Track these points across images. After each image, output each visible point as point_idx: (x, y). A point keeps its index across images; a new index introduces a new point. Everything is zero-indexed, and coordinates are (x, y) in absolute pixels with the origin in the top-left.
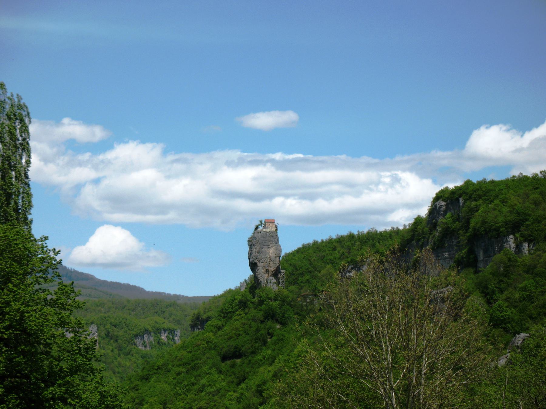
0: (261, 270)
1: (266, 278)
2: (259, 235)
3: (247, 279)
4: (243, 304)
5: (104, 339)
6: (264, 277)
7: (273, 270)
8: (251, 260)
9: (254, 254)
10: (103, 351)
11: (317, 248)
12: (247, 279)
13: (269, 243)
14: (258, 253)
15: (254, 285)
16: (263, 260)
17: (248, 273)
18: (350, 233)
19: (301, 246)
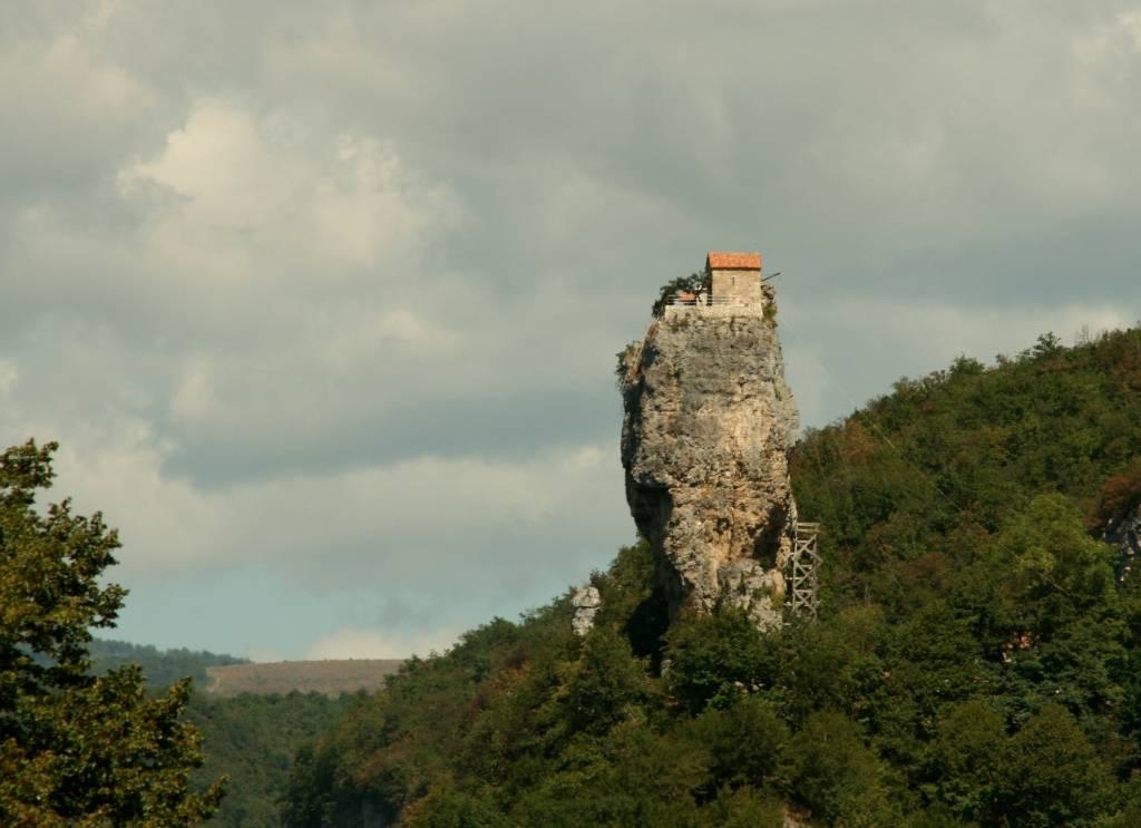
0: (688, 520)
1: (715, 565)
2: (681, 339)
3: (1109, 331)
4: (591, 711)
5: (1007, 748)
6: (708, 559)
7: (754, 520)
8: (637, 470)
9: (652, 439)
10: (179, 713)
11: (977, 401)
12: (1109, 331)
13: (734, 379)
14: (675, 431)
15: (649, 596)
16: (699, 469)
17: (628, 534)
18: (1118, 331)
19: (890, 392)
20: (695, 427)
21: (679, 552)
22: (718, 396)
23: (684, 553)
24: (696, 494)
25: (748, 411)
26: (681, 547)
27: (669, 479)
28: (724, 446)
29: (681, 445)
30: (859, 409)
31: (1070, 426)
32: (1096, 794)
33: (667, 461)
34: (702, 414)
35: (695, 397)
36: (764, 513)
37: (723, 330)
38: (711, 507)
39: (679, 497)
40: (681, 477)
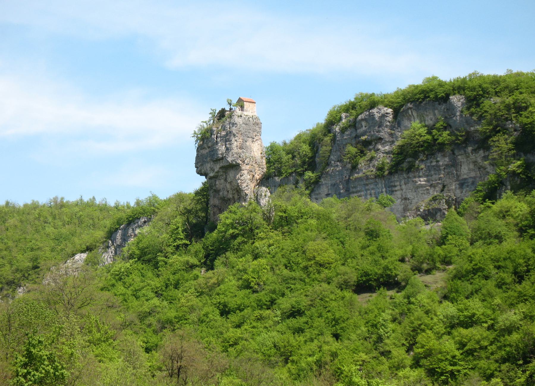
14: (241, 148)
20: (246, 147)
21: (242, 184)
22: (251, 139)
23: (244, 185)
24: (248, 167)
25: (257, 144)
26: (244, 183)
27: (241, 162)
28: (252, 154)
29: (243, 152)
30: (108, 203)
31: (415, 136)
32: (375, 268)
33: (240, 157)
34: (248, 144)
35: (246, 138)
36: (260, 175)
37: (251, 119)
38: (252, 171)
39: (243, 168)
40: (244, 162)
